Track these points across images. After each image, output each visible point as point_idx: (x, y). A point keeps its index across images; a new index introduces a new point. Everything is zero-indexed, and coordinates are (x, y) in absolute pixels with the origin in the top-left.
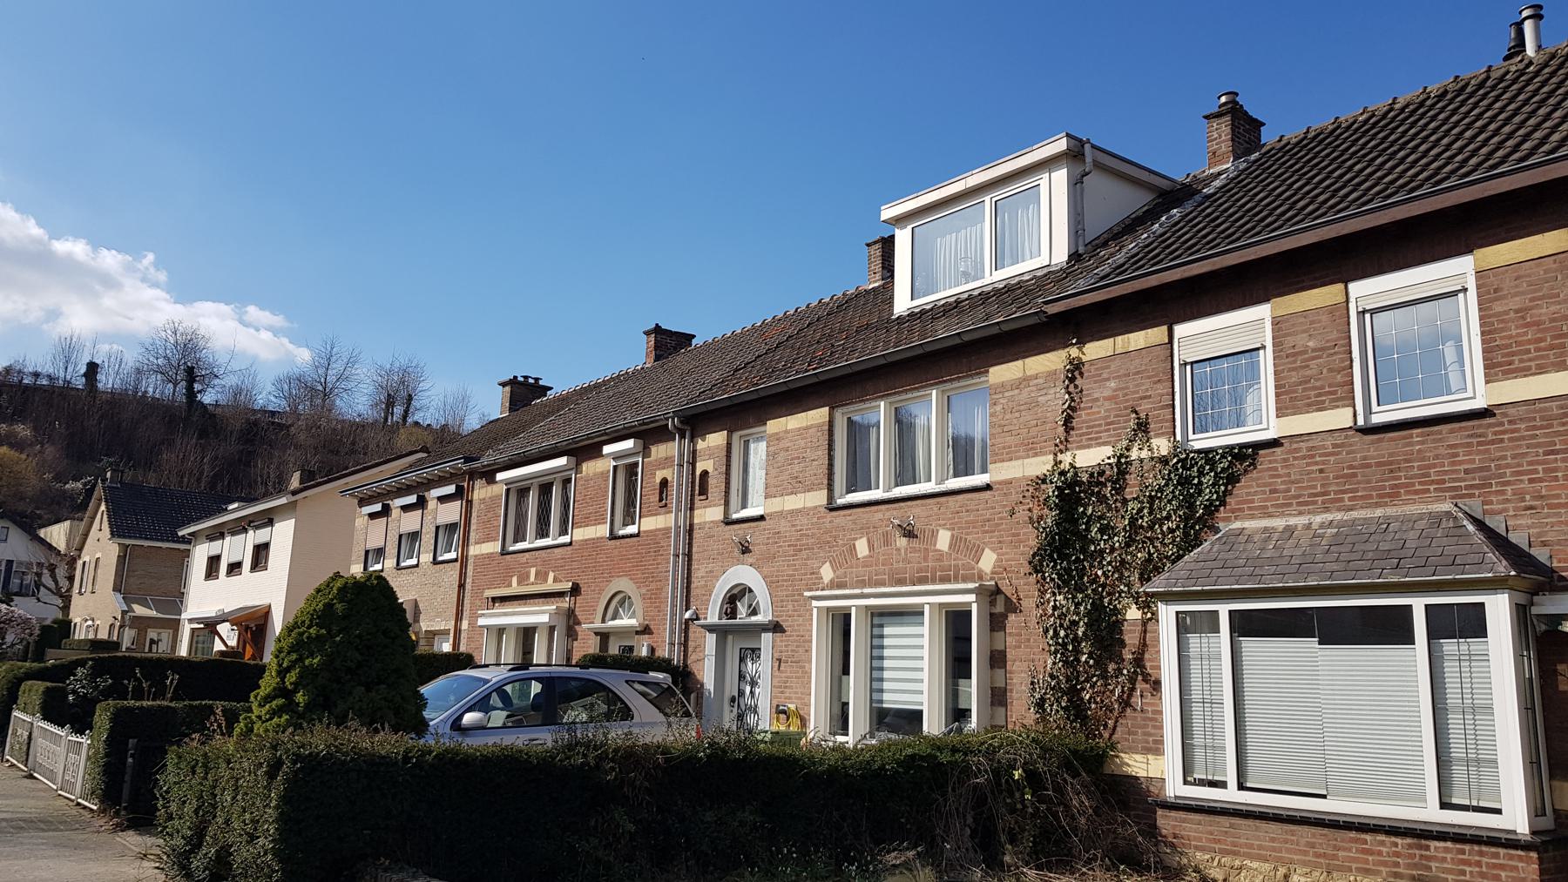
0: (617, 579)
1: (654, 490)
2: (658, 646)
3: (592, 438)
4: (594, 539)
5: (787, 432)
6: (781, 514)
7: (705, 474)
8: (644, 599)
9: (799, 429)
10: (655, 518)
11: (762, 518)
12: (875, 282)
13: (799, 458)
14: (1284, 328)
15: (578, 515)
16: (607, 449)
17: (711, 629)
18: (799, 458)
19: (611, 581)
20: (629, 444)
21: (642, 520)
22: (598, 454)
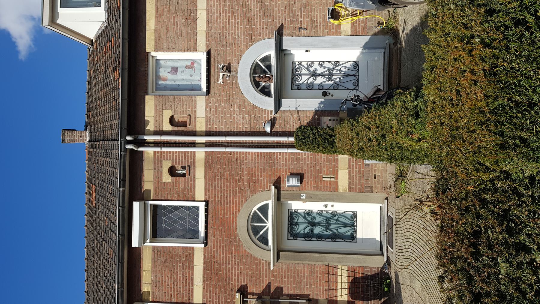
0: (238, 231)
1: (189, 298)
2: (289, 170)
3: (122, 292)
4: (204, 268)
5: (156, 31)
6: (208, 43)
7: (172, 121)
8: (254, 190)
9: (156, 17)
10: (196, 180)
11: (209, 53)
12: (86, 135)
13: (174, 17)
14: (266, 268)
15: (173, 195)
16: (135, 243)
17: (278, 105)
18: (174, 17)
19: (239, 239)
20: (136, 205)
21: (196, 199)
22: (138, 250)
